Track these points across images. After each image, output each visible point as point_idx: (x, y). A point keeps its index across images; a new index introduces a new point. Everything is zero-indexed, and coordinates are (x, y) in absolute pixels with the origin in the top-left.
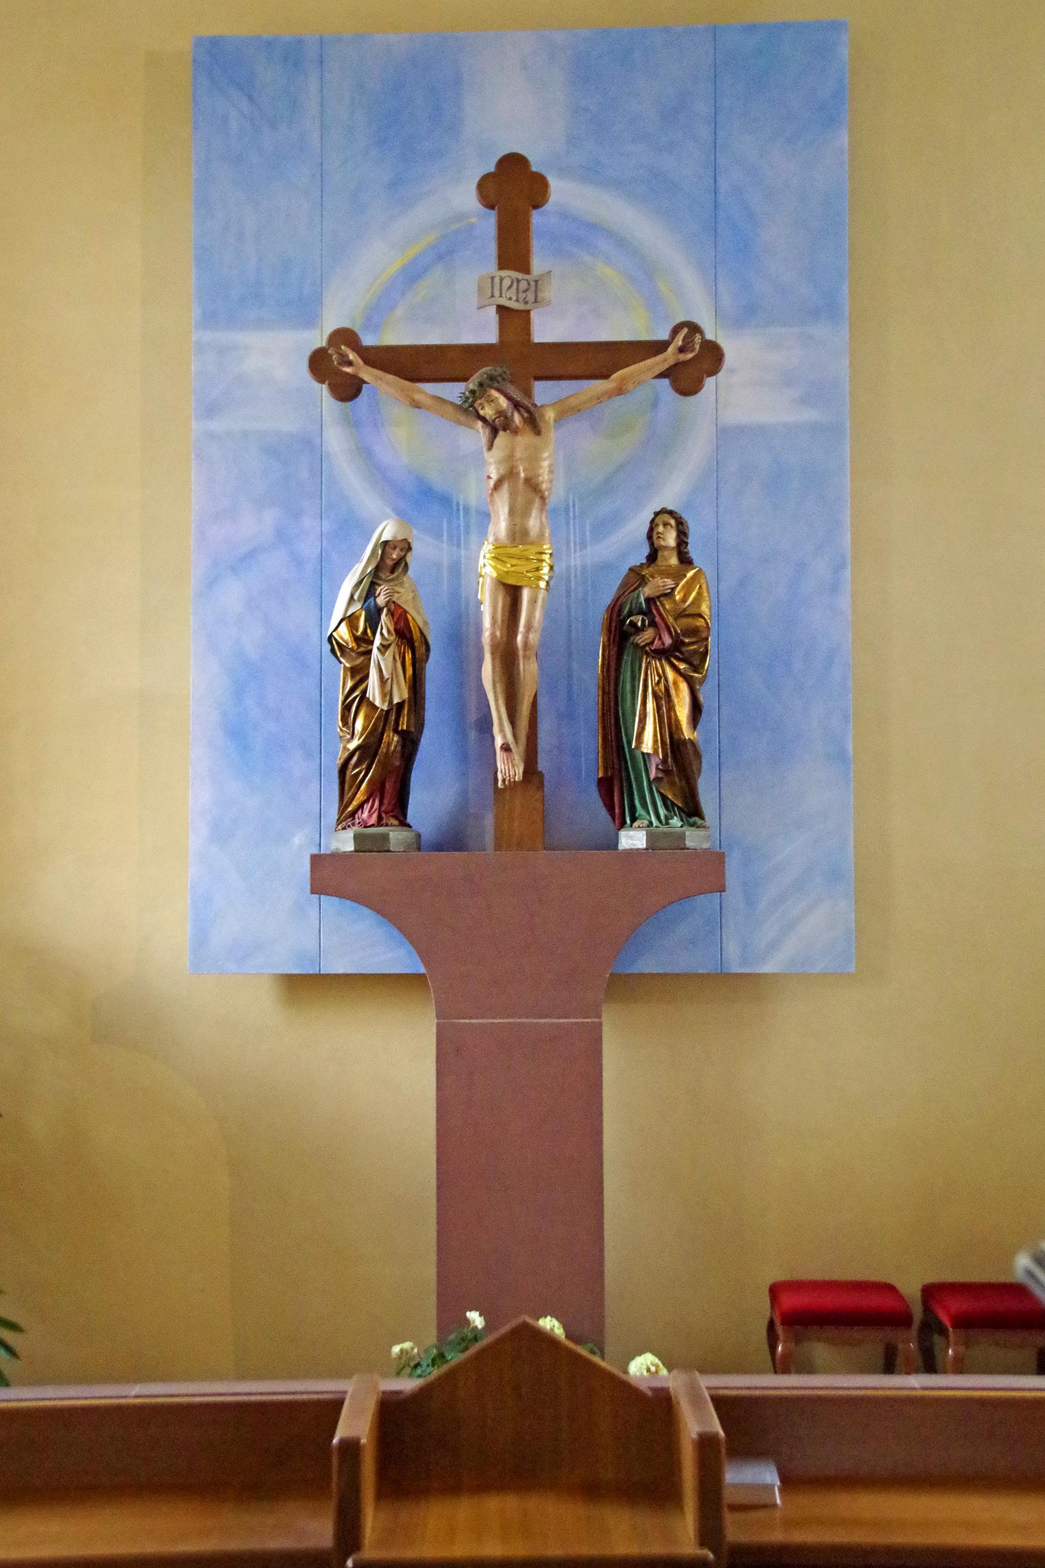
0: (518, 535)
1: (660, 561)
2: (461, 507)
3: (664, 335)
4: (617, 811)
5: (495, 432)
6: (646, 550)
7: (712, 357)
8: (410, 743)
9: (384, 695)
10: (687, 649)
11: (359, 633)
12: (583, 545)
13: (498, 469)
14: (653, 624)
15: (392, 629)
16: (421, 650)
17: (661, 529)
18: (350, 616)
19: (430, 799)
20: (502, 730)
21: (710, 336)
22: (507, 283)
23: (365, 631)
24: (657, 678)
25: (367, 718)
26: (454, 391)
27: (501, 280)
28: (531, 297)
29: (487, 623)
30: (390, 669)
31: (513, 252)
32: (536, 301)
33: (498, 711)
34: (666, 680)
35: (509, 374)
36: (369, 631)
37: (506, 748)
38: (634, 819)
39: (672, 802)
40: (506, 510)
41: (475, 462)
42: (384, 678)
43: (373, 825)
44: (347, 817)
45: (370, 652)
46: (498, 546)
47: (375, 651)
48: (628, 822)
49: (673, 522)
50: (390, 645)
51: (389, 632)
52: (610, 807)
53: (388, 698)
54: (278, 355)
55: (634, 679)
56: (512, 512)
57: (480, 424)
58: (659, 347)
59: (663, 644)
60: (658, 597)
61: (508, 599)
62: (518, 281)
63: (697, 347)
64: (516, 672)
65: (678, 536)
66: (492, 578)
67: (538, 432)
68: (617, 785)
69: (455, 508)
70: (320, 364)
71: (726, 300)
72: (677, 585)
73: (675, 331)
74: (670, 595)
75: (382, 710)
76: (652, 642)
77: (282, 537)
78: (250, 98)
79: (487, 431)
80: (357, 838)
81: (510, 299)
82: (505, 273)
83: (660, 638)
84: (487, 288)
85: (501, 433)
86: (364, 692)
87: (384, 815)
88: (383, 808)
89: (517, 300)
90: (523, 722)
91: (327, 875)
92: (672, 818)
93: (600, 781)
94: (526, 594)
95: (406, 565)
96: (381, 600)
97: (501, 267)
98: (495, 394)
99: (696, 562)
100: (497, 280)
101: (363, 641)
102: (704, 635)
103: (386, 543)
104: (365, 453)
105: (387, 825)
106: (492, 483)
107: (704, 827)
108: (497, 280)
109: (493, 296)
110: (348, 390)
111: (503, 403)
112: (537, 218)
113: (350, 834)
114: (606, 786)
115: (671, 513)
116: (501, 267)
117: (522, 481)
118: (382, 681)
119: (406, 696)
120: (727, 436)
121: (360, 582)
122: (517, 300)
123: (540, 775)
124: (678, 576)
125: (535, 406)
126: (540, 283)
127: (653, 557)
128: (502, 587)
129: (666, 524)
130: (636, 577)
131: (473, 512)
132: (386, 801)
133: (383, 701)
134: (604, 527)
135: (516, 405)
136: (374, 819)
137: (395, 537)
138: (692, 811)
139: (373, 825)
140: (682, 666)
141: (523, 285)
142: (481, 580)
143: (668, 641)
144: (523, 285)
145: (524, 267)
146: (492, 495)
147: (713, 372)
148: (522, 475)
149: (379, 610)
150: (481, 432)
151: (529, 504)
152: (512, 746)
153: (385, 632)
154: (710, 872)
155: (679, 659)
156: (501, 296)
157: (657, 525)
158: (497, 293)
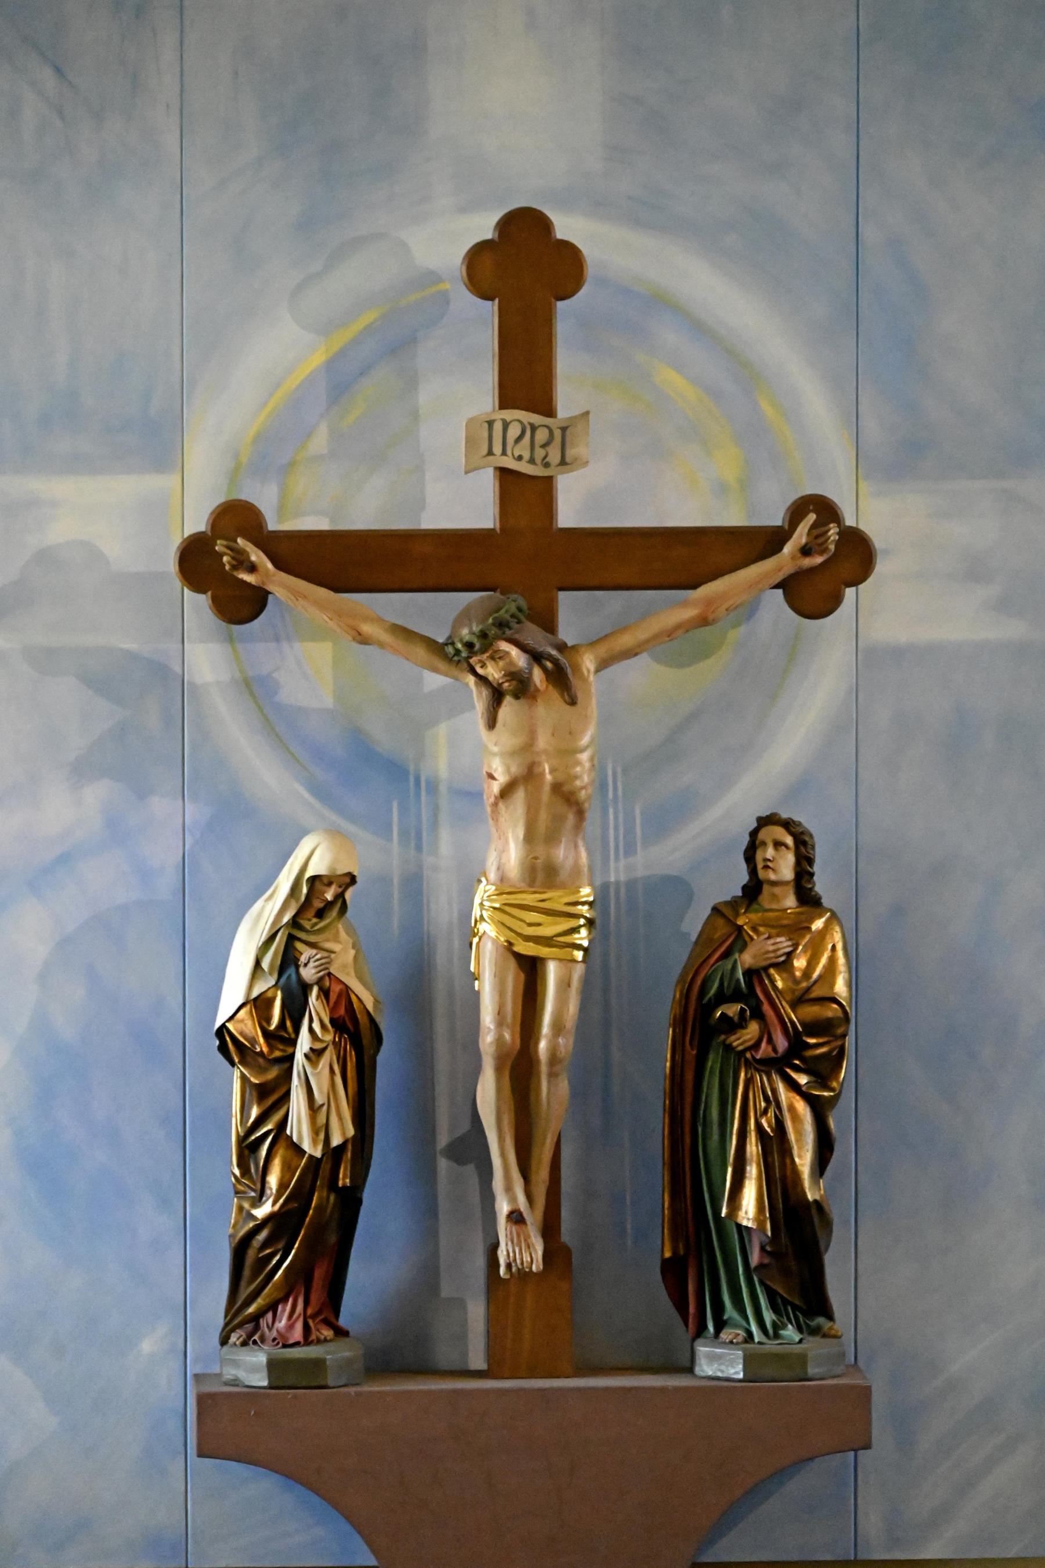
0: (541, 874)
1: (764, 899)
2: (423, 784)
3: (776, 518)
4: (692, 1309)
5: (497, 696)
6: (744, 877)
7: (856, 556)
8: (350, 1203)
9: (315, 1131)
10: (816, 1048)
11: (273, 1027)
12: (630, 849)
13: (508, 770)
14: (758, 1014)
15: (327, 1021)
16: (367, 1039)
17: (770, 852)
18: (256, 999)
19: (372, 1276)
20: (509, 1189)
21: (850, 521)
22: (514, 431)
23: (282, 1024)
24: (763, 1104)
25: (288, 1169)
26: (441, 612)
27: (506, 425)
28: (554, 457)
29: (488, 1018)
30: (325, 1090)
31: (525, 378)
32: (563, 462)
33: (503, 1155)
34: (778, 1106)
35: (519, 582)
36: (288, 1024)
37: (516, 1218)
38: (720, 1325)
39: (782, 1297)
40: (521, 832)
41: (472, 743)
42: (314, 1109)
43: (297, 1344)
44: (242, 1323)
45: (291, 1057)
46: (504, 886)
47: (299, 1058)
48: (711, 1327)
49: (789, 840)
50: (325, 1049)
51: (323, 1026)
52: (681, 1306)
53: (322, 1136)
54: (123, 522)
55: (725, 1104)
56: (530, 838)
57: (471, 680)
58: (769, 541)
59: (775, 1050)
60: (766, 969)
61: (522, 976)
62: (534, 428)
63: (832, 547)
64: (532, 1098)
65: (798, 863)
66: (495, 941)
67: (573, 702)
68: (695, 1264)
69: (412, 779)
70: (197, 562)
71: (872, 428)
72: (796, 946)
73: (798, 510)
74: (785, 965)
75: (311, 1156)
76: (756, 1046)
77: (116, 832)
78: (58, 71)
79: (485, 692)
80: (274, 1366)
81: (520, 458)
82: (509, 414)
83: (770, 1041)
84: (482, 438)
85: (508, 700)
86: (283, 1124)
87: (310, 1322)
88: (309, 1312)
89: (532, 461)
90: (542, 1175)
91: (223, 1427)
92: (784, 1327)
93: (666, 1264)
94: (552, 972)
95: (344, 902)
96: (308, 973)
97: (505, 403)
98: (504, 646)
99: (825, 902)
100: (498, 427)
101: (282, 1039)
102: (840, 1031)
103: (314, 879)
104: (255, 689)
105: (319, 1341)
106: (496, 787)
107: (835, 1337)
108: (498, 427)
109: (490, 453)
110: (240, 605)
111: (518, 658)
112: (566, 313)
113: (259, 1358)
114: (673, 1272)
115: (788, 825)
116: (504, 405)
117: (547, 789)
118: (313, 1108)
119: (351, 1132)
120: (872, 661)
121: (272, 938)
122: (532, 461)
123: (567, 1252)
124: (797, 929)
125: (562, 647)
126: (568, 432)
127: (753, 890)
128: (512, 964)
129: (778, 844)
130: (727, 928)
131: (443, 788)
132: (314, 1297)
133: (315, 1142)
134: (664, 820)
135: (537, 657)
136: (297, 1334)
137: (332, 869)
138: (806, 1298)
139: (297, 1344)
140: (803, 1079)
141: (542, 435)
142: (475, 940)
143: (782, 1043)
144: (542, 435)
145: (543, 404)
146: (495, 805)
147: (856, 581)
148: (549, 777)
149: (305, 988)
150: (479, 699)
151: (558, 820)
152: (526, 1214)
153: (316, 1026)
154: (845, 1421)
155: (797, 1069)
156: (504, 453)
157: (764, 844)
158: (497, 449)
